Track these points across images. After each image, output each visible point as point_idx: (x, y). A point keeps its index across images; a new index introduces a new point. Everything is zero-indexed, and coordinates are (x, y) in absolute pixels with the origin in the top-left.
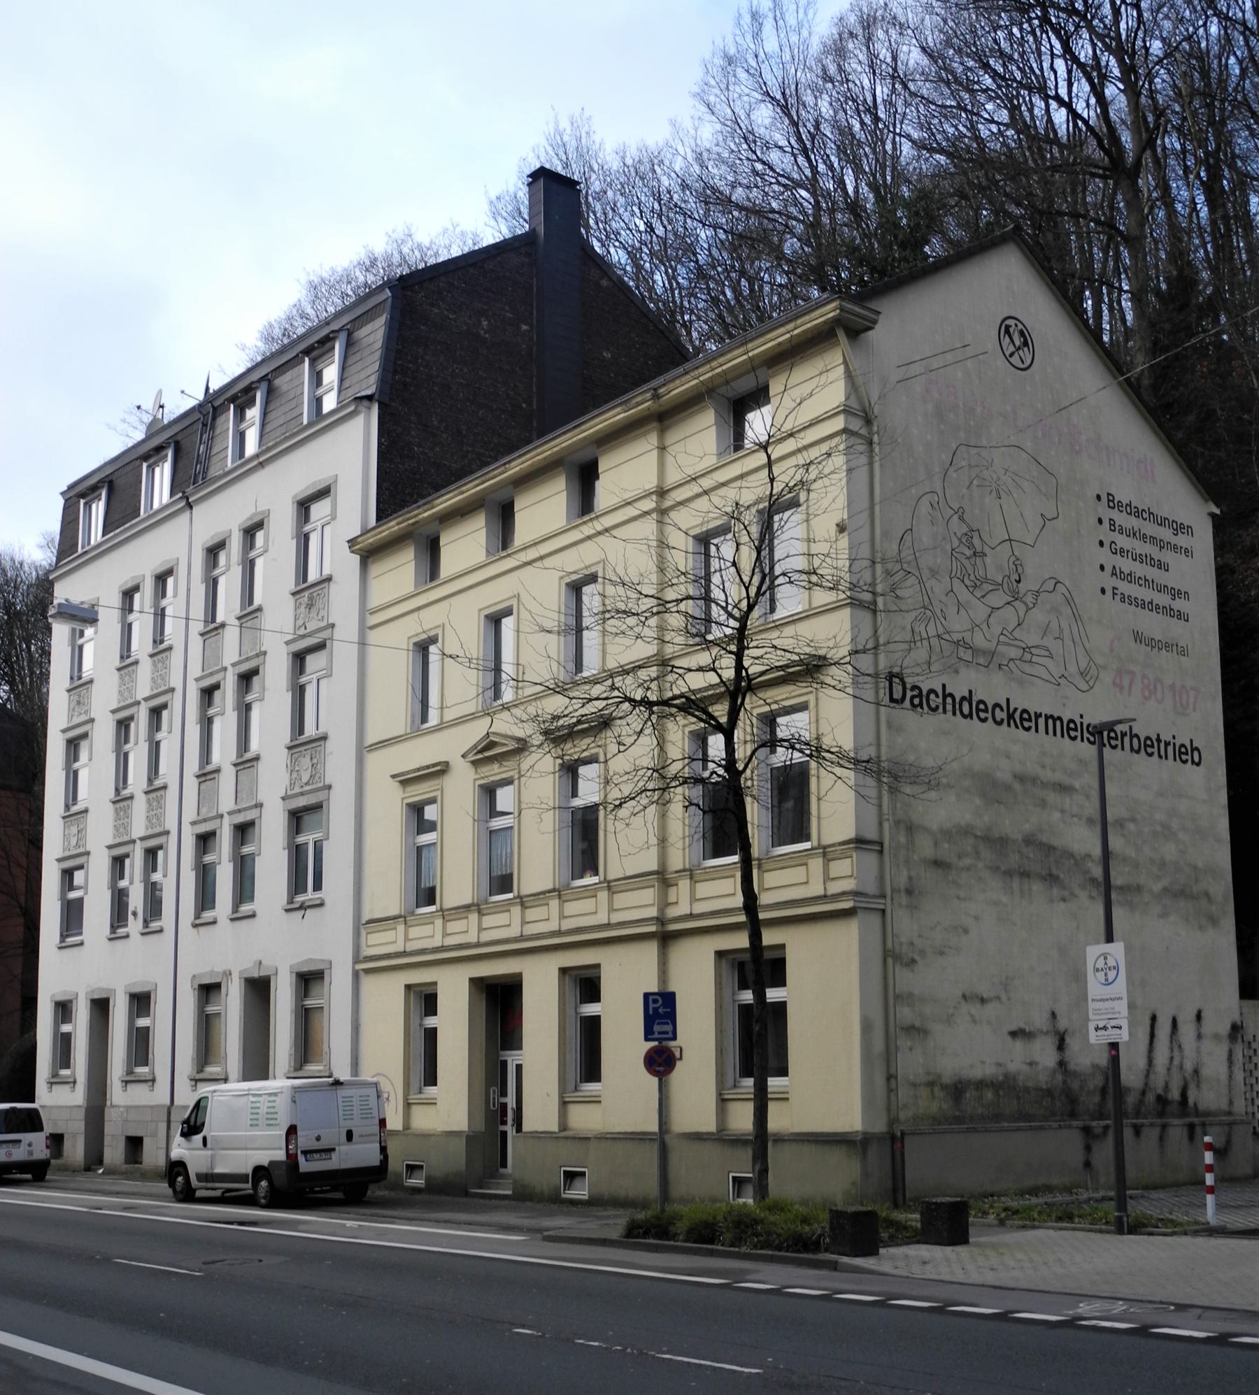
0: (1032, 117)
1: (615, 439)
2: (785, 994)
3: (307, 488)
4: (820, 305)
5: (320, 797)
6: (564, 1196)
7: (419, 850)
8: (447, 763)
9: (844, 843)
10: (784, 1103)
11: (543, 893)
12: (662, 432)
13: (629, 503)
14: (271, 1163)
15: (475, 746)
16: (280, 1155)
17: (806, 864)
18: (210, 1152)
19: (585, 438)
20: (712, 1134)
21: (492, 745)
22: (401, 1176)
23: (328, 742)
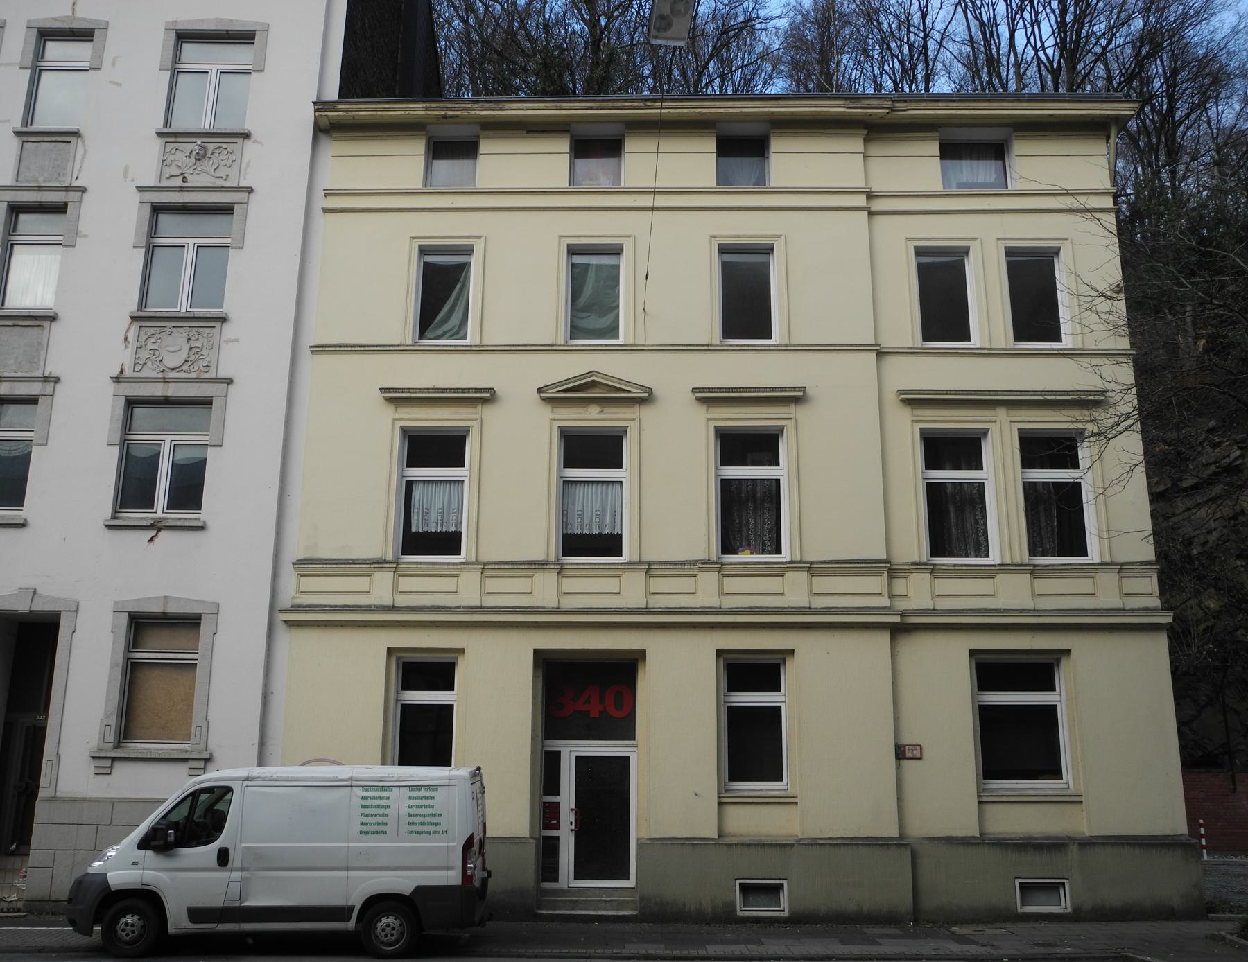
0: (999, 55)
1: (824, 128)
2: (454, 698)
3: (189, 22)
4: (1133, 102)
5: (33, 389)
6: (740, 914)
7: (410, 485)
8: (491, 390)
9: (1141, 563)
10: (793, 807)
11: (695, 563)
12: (867, 140)
13: (1072, 194)
14: (420, 890)
15: (566, 381)
16: (452, 877)
17: (370, 576)
18: (236, 875)
19: (773, 113)
20: (974, 837)
21: (593, 385)
22: (733, 904)
23: (226, 326)
